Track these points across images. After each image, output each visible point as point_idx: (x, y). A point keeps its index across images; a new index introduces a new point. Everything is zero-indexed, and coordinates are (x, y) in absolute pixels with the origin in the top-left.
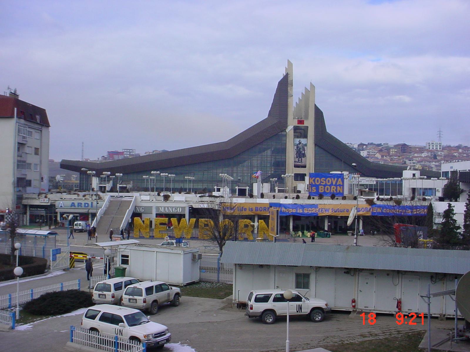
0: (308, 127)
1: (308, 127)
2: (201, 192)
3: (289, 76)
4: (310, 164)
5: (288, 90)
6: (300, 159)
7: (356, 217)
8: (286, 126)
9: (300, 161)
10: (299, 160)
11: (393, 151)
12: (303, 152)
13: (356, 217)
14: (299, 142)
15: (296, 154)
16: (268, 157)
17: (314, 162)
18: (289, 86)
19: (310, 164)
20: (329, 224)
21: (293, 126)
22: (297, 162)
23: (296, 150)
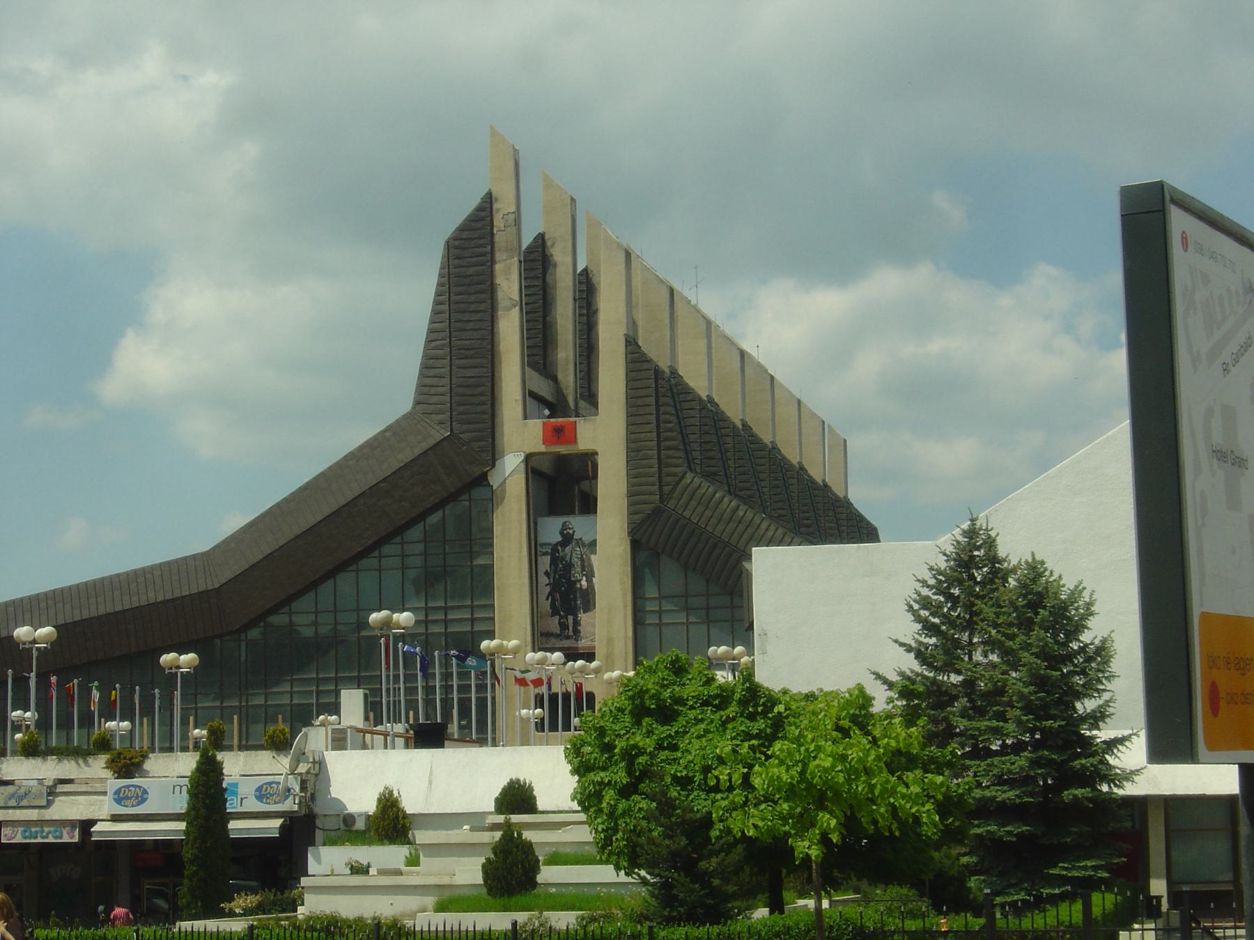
0: (593, 454)
1: (593, 454)
2: (548, 907)
3: (495, 206)
4: (610, 641)
5: (492, 275)
6: (571, 618)
7: (916, 607)
8: (491, 453)
9: (571, 633)
10: (564, 626)
11: (968, 775)
12: (584, 583)
13: (916, 607)
14: (561, 533)
15: (550, 594)
16: (399, 560)
17: (630, 634)
18: (498, 256)
19: (610, 641)
20: (480, 561)
21: (522, 458)
22: (557, 636)
23: (547, 573)
